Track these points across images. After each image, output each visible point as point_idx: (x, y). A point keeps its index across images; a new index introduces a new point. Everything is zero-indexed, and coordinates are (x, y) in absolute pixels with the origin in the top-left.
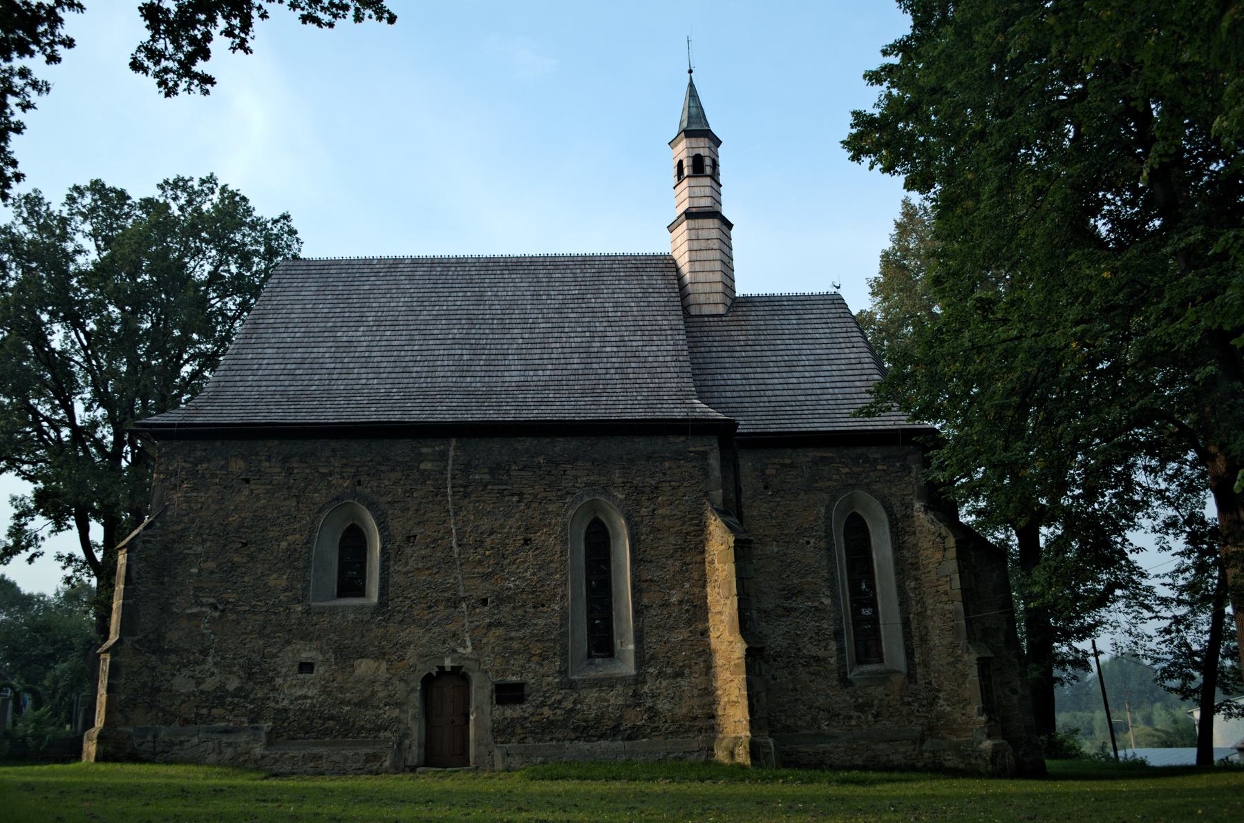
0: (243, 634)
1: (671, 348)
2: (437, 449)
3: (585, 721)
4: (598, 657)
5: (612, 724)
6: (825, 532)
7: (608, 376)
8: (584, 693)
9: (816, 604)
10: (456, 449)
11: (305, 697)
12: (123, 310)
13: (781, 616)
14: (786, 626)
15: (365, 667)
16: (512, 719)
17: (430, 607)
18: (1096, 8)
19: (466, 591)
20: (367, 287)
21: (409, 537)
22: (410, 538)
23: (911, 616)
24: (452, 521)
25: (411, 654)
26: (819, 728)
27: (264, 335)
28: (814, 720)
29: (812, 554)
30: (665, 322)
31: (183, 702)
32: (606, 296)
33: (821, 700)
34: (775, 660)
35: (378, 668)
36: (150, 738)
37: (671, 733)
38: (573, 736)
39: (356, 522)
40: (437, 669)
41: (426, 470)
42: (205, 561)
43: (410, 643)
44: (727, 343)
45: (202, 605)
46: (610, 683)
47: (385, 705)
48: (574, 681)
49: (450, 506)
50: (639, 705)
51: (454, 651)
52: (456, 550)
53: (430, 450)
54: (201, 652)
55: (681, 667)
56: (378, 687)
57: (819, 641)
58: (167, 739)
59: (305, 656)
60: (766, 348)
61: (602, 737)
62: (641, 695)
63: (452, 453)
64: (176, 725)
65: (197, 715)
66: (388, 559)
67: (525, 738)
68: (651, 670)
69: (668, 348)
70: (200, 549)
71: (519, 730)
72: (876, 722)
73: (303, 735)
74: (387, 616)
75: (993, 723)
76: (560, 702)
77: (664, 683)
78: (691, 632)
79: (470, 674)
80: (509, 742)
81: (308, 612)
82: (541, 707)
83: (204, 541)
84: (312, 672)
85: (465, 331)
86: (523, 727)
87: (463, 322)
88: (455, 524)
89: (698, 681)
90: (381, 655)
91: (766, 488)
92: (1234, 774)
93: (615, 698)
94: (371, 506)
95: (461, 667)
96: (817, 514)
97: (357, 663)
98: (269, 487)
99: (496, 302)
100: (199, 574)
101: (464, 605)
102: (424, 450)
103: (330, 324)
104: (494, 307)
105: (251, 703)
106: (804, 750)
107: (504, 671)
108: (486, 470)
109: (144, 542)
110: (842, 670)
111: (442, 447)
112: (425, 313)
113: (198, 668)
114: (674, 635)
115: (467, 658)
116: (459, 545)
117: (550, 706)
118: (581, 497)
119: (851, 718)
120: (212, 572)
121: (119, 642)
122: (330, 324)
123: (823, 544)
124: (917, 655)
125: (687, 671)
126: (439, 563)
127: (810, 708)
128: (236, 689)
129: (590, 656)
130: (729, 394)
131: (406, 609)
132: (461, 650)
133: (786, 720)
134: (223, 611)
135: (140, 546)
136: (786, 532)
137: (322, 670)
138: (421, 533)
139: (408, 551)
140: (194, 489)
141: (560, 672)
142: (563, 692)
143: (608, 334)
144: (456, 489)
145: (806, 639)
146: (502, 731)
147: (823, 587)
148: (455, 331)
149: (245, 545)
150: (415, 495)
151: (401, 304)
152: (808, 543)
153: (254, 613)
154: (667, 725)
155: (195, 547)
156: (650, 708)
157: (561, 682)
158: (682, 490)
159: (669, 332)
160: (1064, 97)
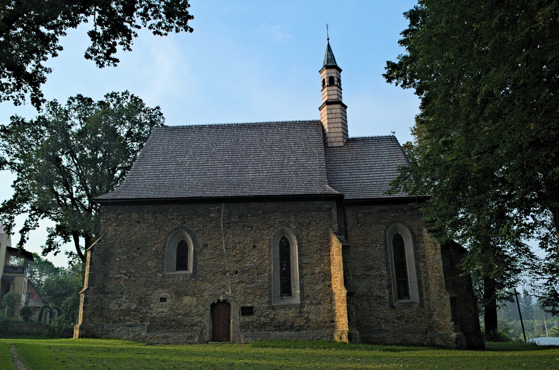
9: (380, 273)
15: (187, 300)
56: (192, 308)
63: (223, 210)
65: (119, 319)
68: (307, 302)
86: (252, 325)
90: (194, 295)
97: (184, 298)
105: (141, 314)
158: (320, 224)
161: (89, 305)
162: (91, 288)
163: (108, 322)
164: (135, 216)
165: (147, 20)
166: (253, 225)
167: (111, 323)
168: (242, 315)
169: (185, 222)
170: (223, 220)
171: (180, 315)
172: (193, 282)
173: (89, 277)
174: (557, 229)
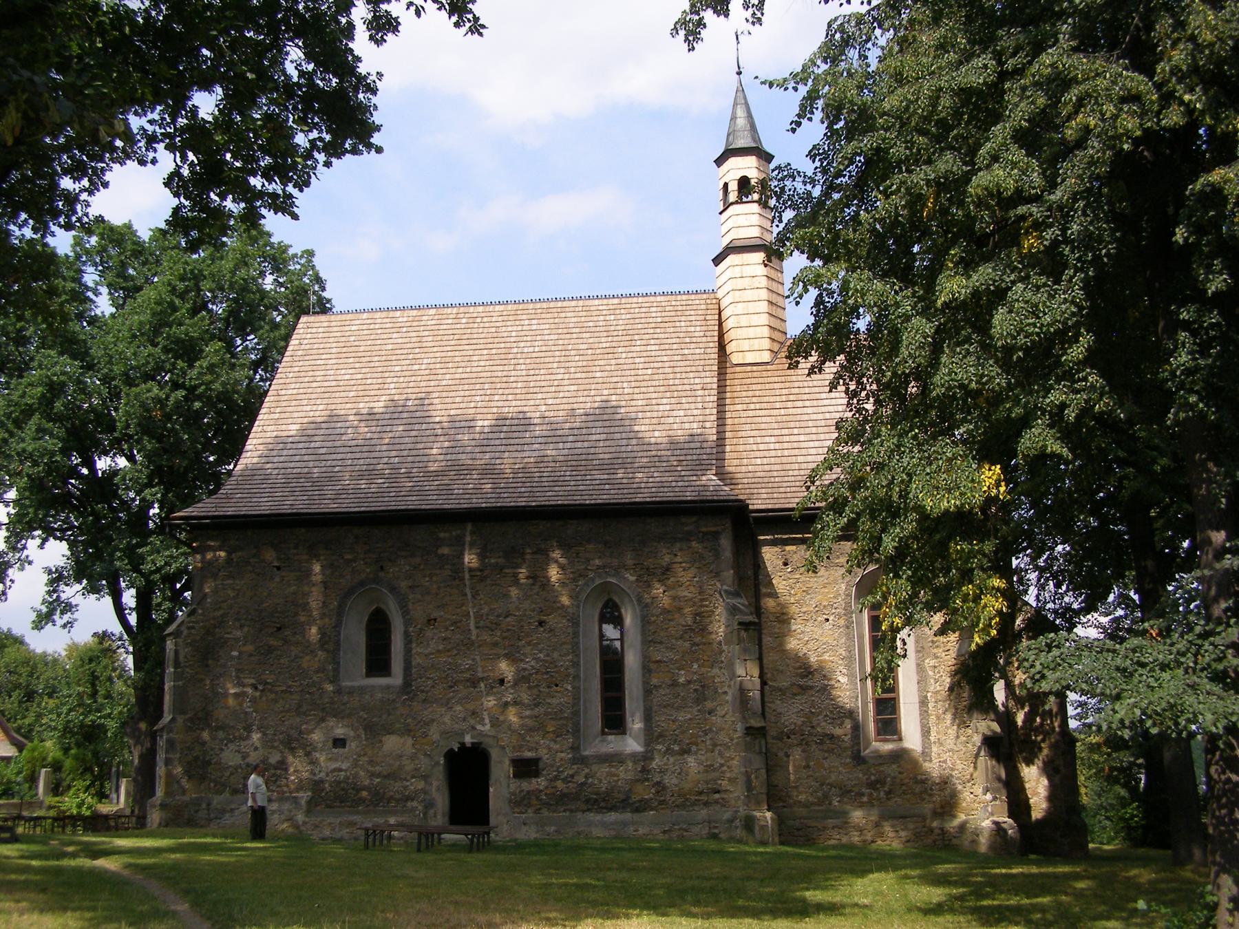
0: (282, 712)
1: (699, 412)
2: (454, 533)
3: (597, 794)
4: (611, 734)
5: (622, 797)
6: (845, 609)
7: (629, 448)
8: (595, 768)
10: (473, 533)
11: (340, 770)
13: (795, 695)
14: (801, 704)
15: (392, 743)
16: (528, 792)
17: (451, 687)
19: (484, 672)
20: (390, 347)
21: (429, 620)
22: (431, 621)
23: (929, 695)
24: (471, 604)
25: (434, 733)
26: (830, 804)
28: (826, 796)
29: (830, 632)
30: (697, 381)
31: (232, 774)
32: (638, 349)
33: (833, 777)
34: (789, 737)
35: (404, 744)
36: (204, 806)
37: (677, 806)
38: (586, 808)
39: (383, 606)
40: (458, 745)
41: (443, 555)
42: (244, 645)
43: (433, 720)
44: (766, 399)
45: (244, 686)
46: (615, 759)
47: (412, 778)
48: (586, 757)
49: (468, 591)
50: (647, 780)
51: (474, 728)
52: (474, 632)
53: (447, 535)
54: (245, 729)
55: (688, 744)
56: (405, 761)
57: (833, 719)
58: (219, 807)
59: (340, 732)
60: (807, 403)
61: (612, 808)
62: (649, 771)
64: (227, 795)
66: (410, 642)
67: (540, 809)
69: (695, 412)
71: (534, 802)
72: (888, 799)
73: (338, 804)
74: (411, 695)
75: (998, 802)
76: (572, 776)
77: (672, 760)
78: (699, 711)
79: (490, 750)
80: (526, 812)
81: (339, 691)
82: (555, 781)
83: (242, 626)
84: (344, 747)
85: (487, 398)
86: (538, 799)
87: (486, 386)
88: (474, 607)
89: (703, 758)
90: (408, 731)
91: (786, 564)
93: (625, 773)
94: (393, 589)
95: (481, 743)
96: (837, 591)
98: (298, 574)
99: (521, 361)
100: (239, 657)
101: (482, 685)
102: (442, 535)
103: (352, 394)
104: (519, 367)
106: (813, 824)
107: (521, 746)
108: (501, 554)
109: (189, 628)
110: (856, 748)
111: (459, 532)
112: (448, 377)
113: (243, 743)
114: (682, 714)
115: (486, 735)
116: (477, 628)
117: (564, 780)
118: (593, 580)
119: (863, 795)
120: (251, 655)
121: (173, 720)
122: (352, 394)
123: (842, 622)
124: (933, 734)
125: (694, 748)
126: (458, 645)
127: (822, 785)
128: (278, 762)
129: (603, 733)
130: (759, 461)
131: (428, 689)
132: (479, 727)
133: (797, 796)
134: (262, 691)
135: (185, 632)
136: (804, 609)
137: (353, 745)
138: (441, 617)
139: (429, 633)
140: (230, 577)
141: (572, 748)
142: (575, 767)
143: (635, 397)
144: (473, 573)
145: (820, 718)
146: (520, 802)
147: (841, 665)
148: (478, 398)
149: (279, 629)
150: (434, 579)
151: (423, 367)
152: (828, 620)
154: (673, 799)
155: (234, 632)
156: (658, 783)
157: (574, 758)
159: (700, 393)
162: (180, 719)
169: (382, 568)
171: (378, 776)
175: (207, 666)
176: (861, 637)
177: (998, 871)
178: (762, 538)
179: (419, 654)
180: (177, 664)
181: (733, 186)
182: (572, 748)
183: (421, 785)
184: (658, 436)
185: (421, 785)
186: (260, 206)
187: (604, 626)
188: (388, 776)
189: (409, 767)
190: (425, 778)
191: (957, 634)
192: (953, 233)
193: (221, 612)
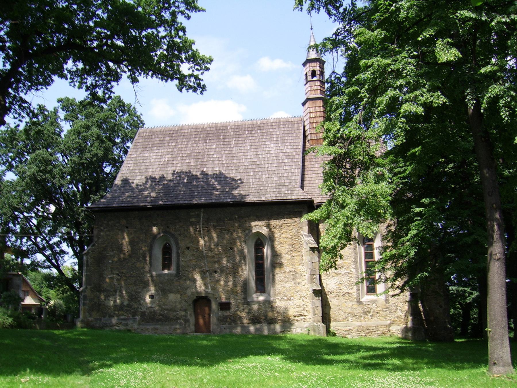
9: (349, 271)
10: (204, 213)
12: (510, 55)
15: (172, 297)
18: (130, 48)
27: (312, 169)
45: (114, 274)
56: (177, 304)
63: (202, 215)
65: (114, 313)
68: (278, 297)
70: (112, 254)
86: (230, 319)
90: (178, 292)
92: (324, 367)
97: (169, 295)
105: (133, 309)
141: (244, 298)
153: (132, 277)
158: (292, 227)
160: (111, 64)
161: (88, 302)
162: (89, 287)
163: (104, 317)
164: (124, 222)
165: (198, 329)
166: (230, 229)
167: (107, 317)
168: (221, 310)
169: (168, 227)
170: (203, 224)
171: (167, 310)
172: (177, 281)
173: (236, 357)
174: (500, 113)
175: (99, 266)
176: (360, 253)
177: (423, 316)
178: (457, 340)
179: (182, 261)
180: (87, 265)
181: (310, 74)
182: (244, 298)
183: (183, 313)
184: (397, 330)
185: (183, 313)
186: (22, 261)
187: (320, 288)
188: (170, 310)
189: (179, 306)
190: (185, 310)
191: (507, 67)
192: (460, 186)
193: (105, 245)
